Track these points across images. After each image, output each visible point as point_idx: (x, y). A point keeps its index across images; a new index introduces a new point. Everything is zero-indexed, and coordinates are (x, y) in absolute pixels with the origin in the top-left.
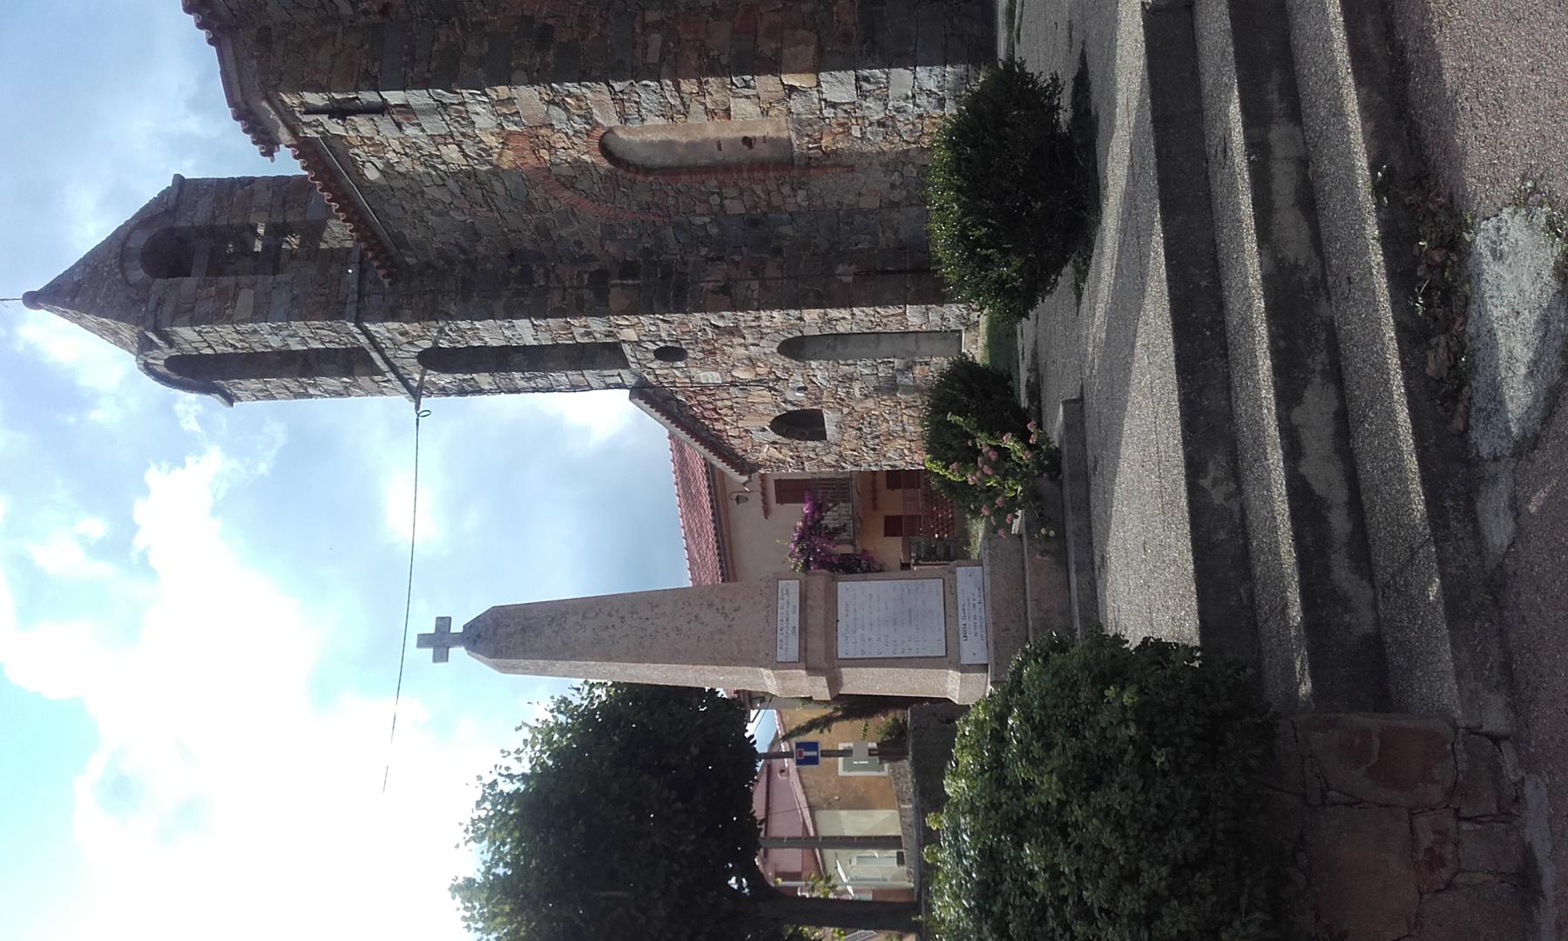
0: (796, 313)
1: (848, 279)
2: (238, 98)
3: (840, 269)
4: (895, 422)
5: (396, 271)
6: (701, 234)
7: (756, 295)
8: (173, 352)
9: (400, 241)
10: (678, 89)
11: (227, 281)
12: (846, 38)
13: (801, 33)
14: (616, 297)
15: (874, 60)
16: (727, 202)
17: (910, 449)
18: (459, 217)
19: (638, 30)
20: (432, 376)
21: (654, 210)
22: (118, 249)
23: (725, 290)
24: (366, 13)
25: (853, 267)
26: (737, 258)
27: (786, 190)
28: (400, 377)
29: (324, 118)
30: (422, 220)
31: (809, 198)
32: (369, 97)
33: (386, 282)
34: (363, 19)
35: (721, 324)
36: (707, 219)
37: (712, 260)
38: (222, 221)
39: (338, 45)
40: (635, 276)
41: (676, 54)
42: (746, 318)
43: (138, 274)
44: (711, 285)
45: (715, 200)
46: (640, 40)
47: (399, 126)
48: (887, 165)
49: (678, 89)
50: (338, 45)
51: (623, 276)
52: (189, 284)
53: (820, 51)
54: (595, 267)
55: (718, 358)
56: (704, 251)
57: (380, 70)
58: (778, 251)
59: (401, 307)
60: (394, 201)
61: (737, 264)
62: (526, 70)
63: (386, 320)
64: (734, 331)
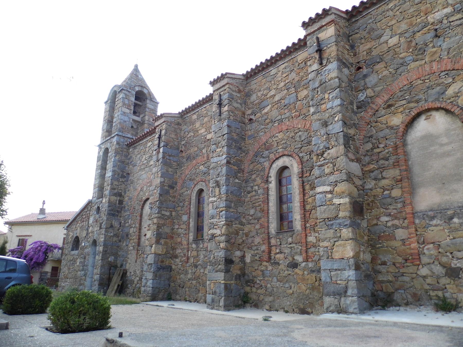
0: (102, 245)
1: (110, 259)
2: (165, 115)
3: (113, 257)
4: (72, 271)
5: (130, 145)
6: (127, 221)
7: (109, 234)
8: (117, 92)
9: (135, 148)
10: (155, 218)
11: (132, 108)
12: (162, 262)
13: (165, 250)
14: (114, 198)
15: (155, 269)
16: (133, 229)
17: (65, 274)
18: (138, 162)
19: (171, 210)
20: (103, 150)
21: (134, 210)
22: (143, 85)
23: (112, 226)
24: (182, 147)
25: (113, 261)
26: (120, 230)
27: (133, 244)
28: (103, 143)
29: (159, 134)
30: (139, 154)
31: (131, 250)
32: (162, 144)
33: (126, 143)
34: (181, 146)
35: (103, 225)
36: (130, 223)
37: (120, 224)
38: (147, 110)
39: (175, 140)
40: (119, 204)
41: (163, 218)
42: (103, 231)
43: (137, 89)
44: (114, 223)
45: (134, 226)
46: (168, 210)
47: (155, 150)
48: (135, 271)
49: (155, 218)
50: (175, 140)
51: (120, 201)
52: (133, 99)
53: (160, 255)
54: (123, 194)
55: (95, 223)
56: (123, 222)
57: (168, 148)
58: (120, 241)
59: (119, 146)
60: (144, 148)
61: (118, 230)
62: (164, 182)
63: (117, 141)
64: (101, 228)
